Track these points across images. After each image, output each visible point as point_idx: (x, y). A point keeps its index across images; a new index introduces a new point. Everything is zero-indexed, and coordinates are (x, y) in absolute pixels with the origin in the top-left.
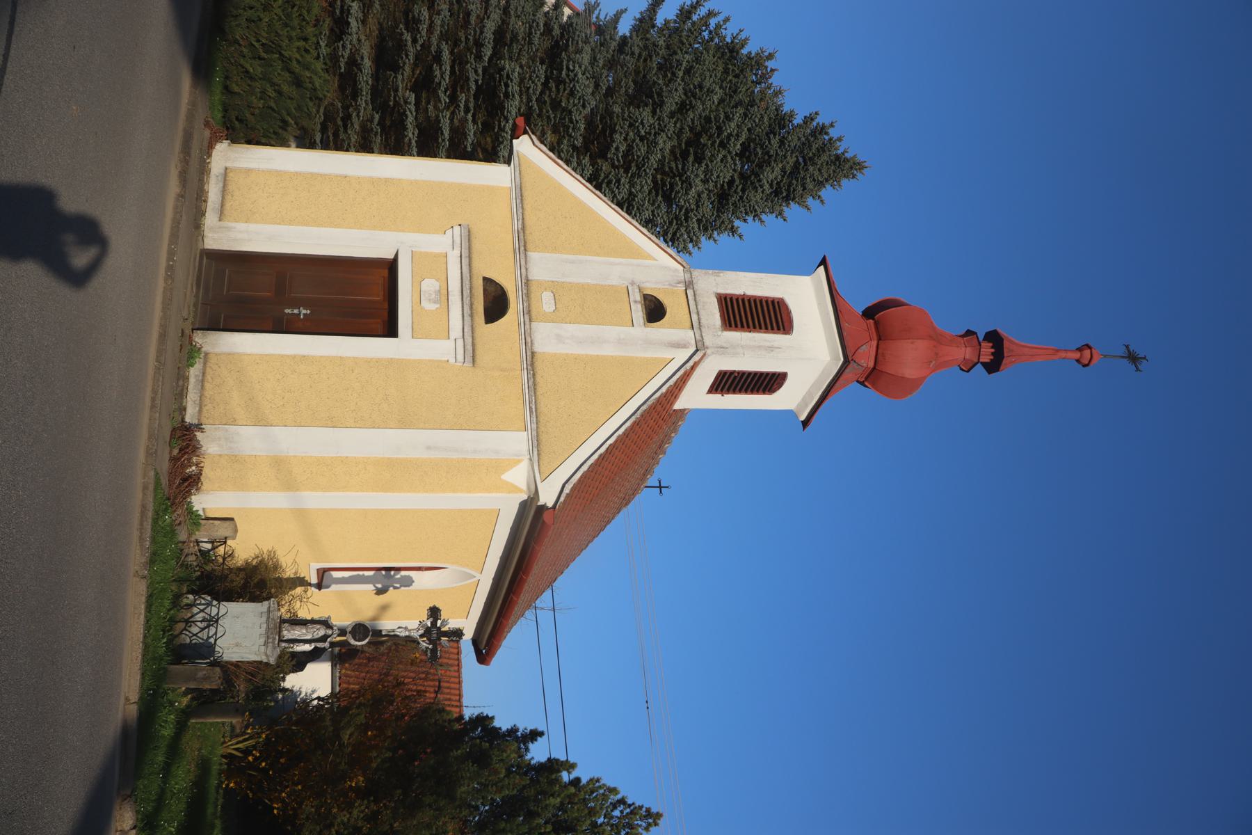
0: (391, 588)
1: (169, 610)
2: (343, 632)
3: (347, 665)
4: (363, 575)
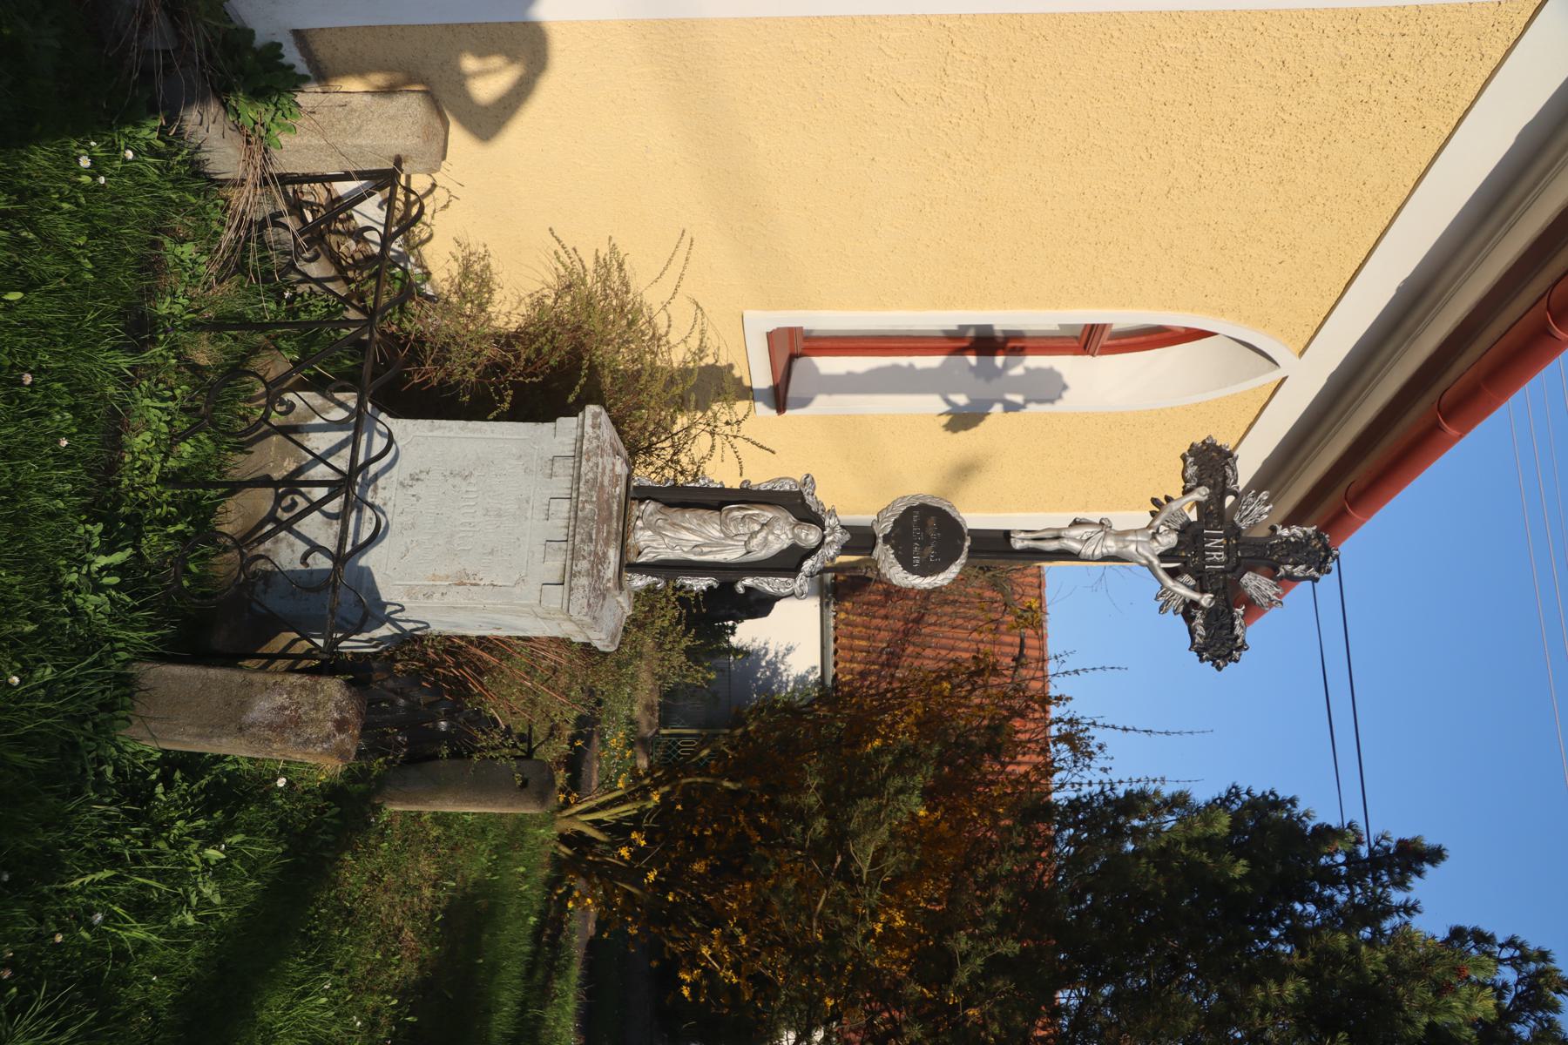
0: (997, 408)
1: (177, 438)
2: (860, 539)
3: (848, 605)
4: (911, 366)
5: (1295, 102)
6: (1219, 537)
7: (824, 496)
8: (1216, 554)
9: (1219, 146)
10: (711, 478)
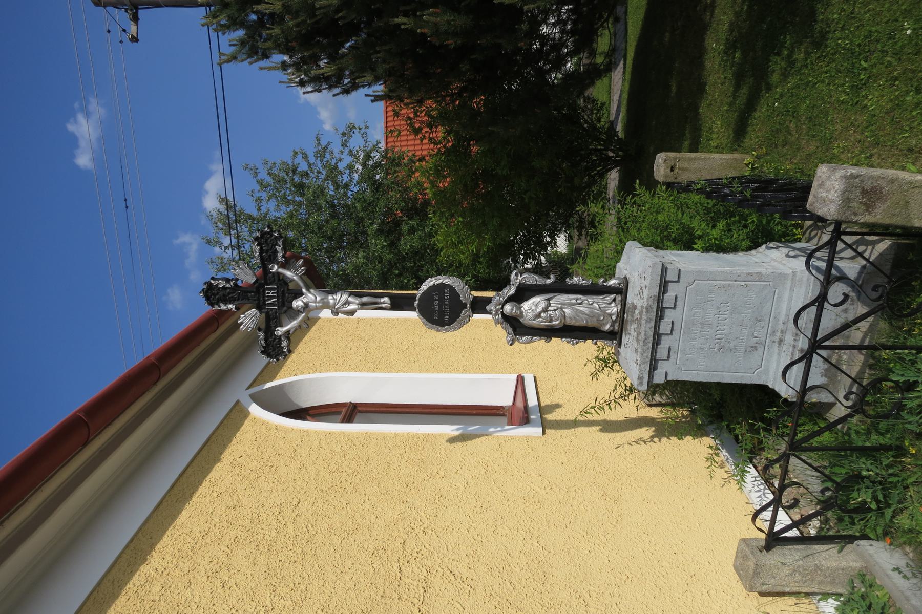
2: (479, 306)
5: (220, 559)
6: (269, 305)
7: (501, 333)
8: (271, 295)
9: (267, 532)
10: (569, 344)
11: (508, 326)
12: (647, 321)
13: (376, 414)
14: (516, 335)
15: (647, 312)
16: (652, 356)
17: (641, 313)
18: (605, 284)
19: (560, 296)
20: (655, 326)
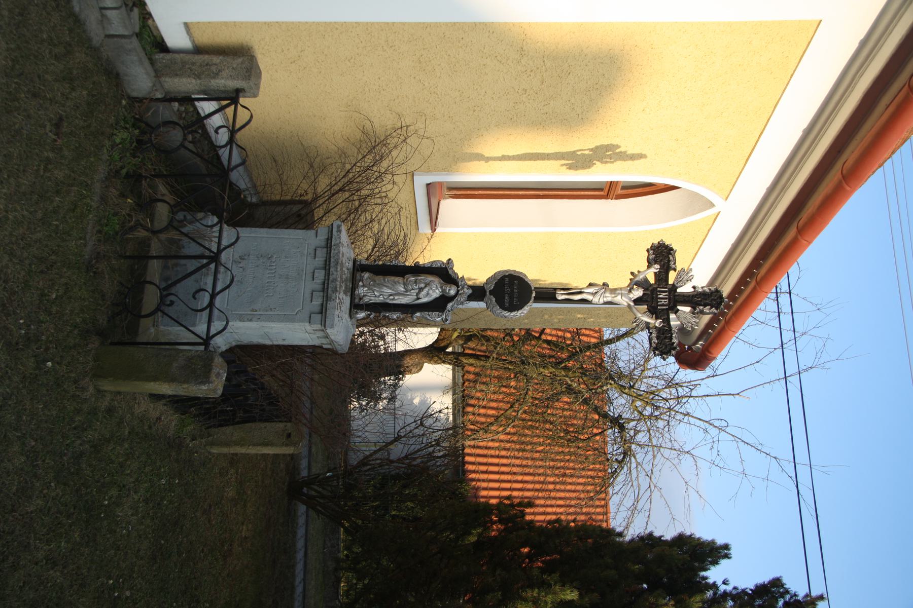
7: (460, 270)
11: (453, 275)
12: (336, 280)
13: (585, 188)
14: (446, 268)
15: (336, 287)
16: (331, 250)
17: (341, 287)
18: (369, 313)
19: (408, 302)
20: (329, 276)
